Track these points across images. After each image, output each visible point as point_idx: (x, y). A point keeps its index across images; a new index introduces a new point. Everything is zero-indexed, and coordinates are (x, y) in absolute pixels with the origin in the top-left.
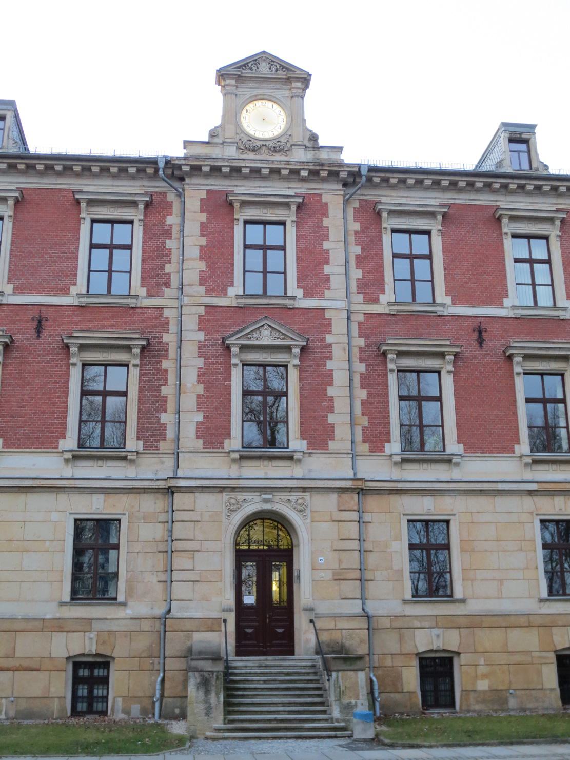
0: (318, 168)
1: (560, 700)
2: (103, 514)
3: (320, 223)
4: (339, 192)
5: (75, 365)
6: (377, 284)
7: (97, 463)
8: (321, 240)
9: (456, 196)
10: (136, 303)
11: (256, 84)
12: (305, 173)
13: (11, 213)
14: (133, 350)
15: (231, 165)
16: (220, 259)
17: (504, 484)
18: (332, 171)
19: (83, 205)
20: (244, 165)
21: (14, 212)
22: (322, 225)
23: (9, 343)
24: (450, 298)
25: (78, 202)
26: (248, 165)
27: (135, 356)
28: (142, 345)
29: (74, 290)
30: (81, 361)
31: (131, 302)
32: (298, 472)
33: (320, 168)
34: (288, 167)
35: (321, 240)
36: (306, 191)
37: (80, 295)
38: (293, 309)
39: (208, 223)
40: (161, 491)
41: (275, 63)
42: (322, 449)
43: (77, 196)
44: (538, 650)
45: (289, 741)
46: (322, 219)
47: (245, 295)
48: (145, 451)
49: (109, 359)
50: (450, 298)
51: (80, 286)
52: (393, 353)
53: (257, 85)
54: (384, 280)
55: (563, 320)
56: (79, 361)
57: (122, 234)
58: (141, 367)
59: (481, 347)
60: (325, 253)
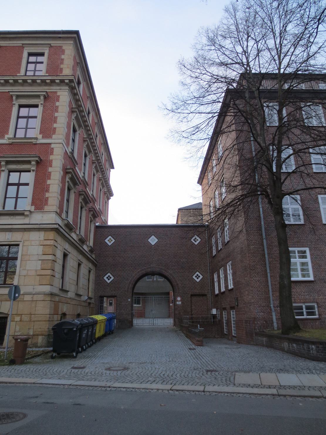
1: (5, 340)
5: (3, 171)
7: (11, 217)
9: (39, 88)
10: (36, 142)
13: (42, 102)
14: (32, 163)
17: (6, 226)
19: (14, 98)
21: (44, 102)
23: (39, 161)
24: (41, 136)
25: (12, 96)
26: (21, 78)
27: (33, 165)
28: (36, 160)
29: (6, 136)
30: (7, 169)
31: (34, 141)
32: (26, 221)
37: (9, 139)
38: (36, 144)
40: (55, 229)
42: (39, 210)
43: (11, 94)
44: (53, 313)
47: (25, 138)
48: (35, 211)
49: (21, 168)
50: (41, 136)
51: (11, 134)
52: (4, 162)
55: (35, 144)
56: (6, 169)
57: (33, 112)
58: (37, 171)
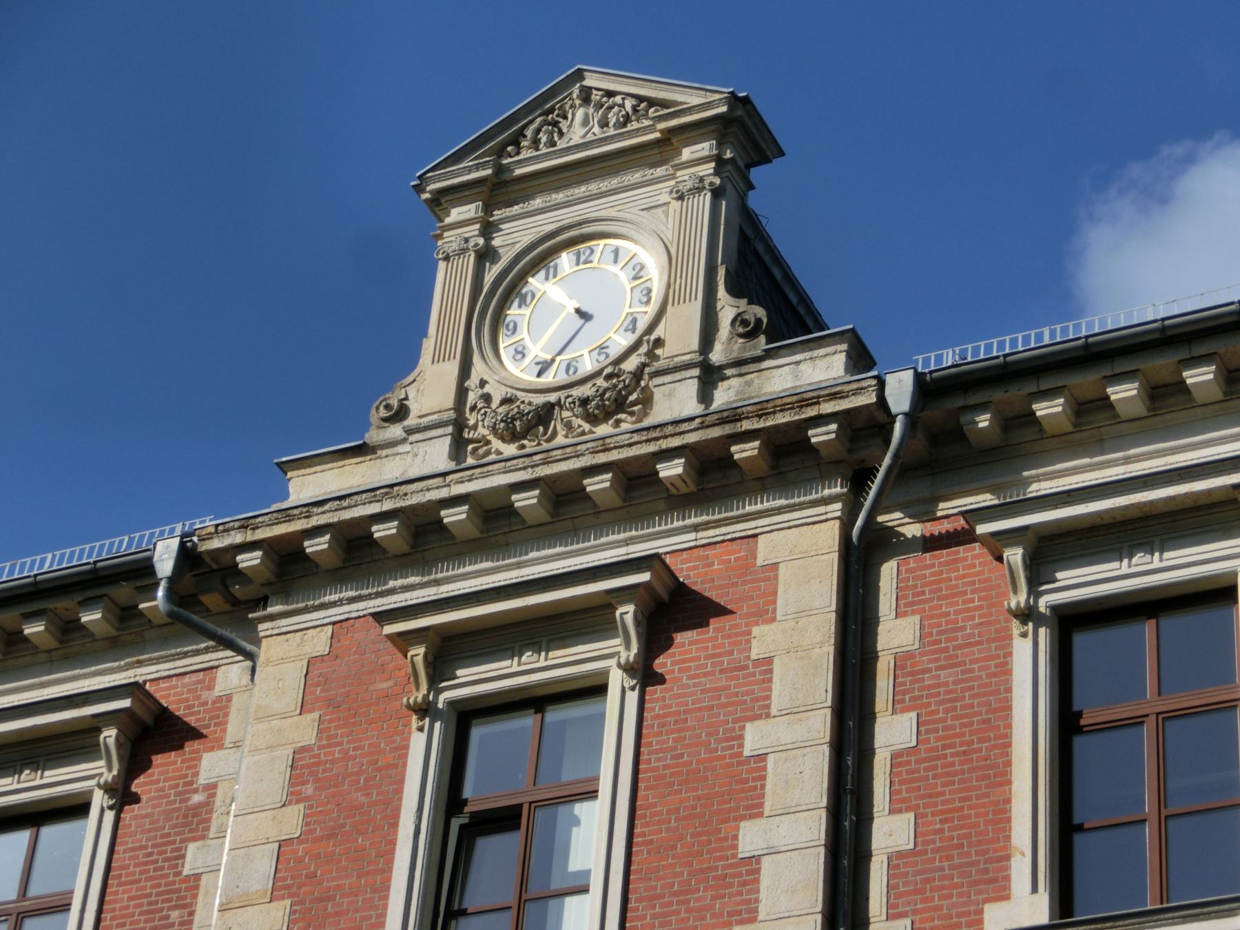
0: (716, 432)
2: (178, 668)
3: (740, 651)
4: (821, 509)
6: (977, 863)
8: (920, 853)
11: (557, 193)
12: (677, 466)
15: (400, 504)
16: (347, 877)
18: (777, 428)
20: (443, 493)
22: (748, 658)
33: (727, 429)
34: (602, 458)
35: (920, 853)
36: (692, 536)
39: (320, 748)
41: (618, 99)
45: (274, 527)
46: (749, 633)
53: (561, 195)
54: (1008, 838)
59: (731, 612)
60: (749, 771)
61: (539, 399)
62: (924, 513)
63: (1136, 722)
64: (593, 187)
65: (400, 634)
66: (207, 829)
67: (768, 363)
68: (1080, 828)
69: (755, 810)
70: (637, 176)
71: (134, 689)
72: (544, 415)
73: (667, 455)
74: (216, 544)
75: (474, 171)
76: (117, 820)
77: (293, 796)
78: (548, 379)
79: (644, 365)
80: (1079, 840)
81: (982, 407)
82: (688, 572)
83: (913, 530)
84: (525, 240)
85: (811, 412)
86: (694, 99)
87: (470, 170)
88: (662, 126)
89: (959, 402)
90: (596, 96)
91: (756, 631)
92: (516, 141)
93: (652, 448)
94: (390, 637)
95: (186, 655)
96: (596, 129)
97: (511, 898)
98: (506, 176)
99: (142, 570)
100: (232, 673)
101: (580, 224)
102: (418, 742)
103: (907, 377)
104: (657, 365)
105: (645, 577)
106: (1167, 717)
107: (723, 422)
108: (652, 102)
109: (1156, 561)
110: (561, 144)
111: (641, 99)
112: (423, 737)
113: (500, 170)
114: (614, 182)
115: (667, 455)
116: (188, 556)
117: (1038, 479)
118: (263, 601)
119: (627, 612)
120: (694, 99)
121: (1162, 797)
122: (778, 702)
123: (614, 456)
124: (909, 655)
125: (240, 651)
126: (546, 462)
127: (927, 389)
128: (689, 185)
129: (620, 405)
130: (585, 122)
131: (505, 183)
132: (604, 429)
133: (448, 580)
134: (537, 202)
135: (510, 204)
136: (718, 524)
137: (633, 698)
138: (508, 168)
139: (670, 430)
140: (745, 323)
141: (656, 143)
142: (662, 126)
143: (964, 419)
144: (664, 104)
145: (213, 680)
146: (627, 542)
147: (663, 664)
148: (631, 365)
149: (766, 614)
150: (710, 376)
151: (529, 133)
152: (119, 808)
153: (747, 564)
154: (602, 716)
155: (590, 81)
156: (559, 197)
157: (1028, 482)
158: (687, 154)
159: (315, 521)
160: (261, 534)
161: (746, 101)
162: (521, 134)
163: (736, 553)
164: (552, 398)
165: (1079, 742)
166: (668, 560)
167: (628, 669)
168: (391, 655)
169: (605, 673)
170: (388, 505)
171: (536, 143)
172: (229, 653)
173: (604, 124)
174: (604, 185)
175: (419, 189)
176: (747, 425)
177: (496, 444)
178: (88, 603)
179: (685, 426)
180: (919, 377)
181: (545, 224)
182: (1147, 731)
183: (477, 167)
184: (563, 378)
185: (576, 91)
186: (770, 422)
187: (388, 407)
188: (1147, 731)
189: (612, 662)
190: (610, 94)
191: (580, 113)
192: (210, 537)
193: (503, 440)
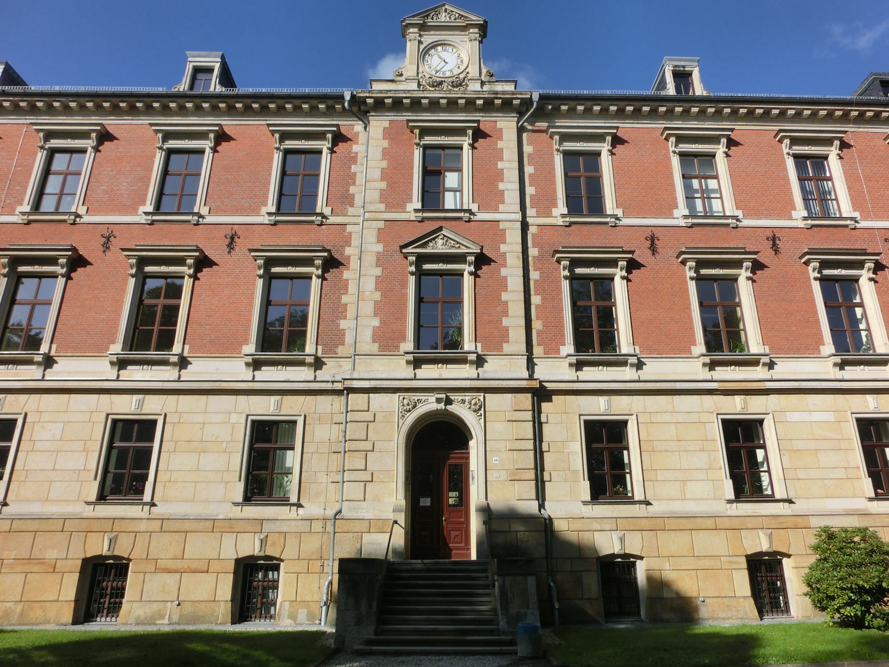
0: (492, 96)
20: (423, 95)
33: (495, 96)
34: (464, 96)
41: (454, 13)
61: (441, 79)
62: (532, 124)
63: (298, 175)
64: (447, 33)
65: (156, 130)
66: (357, 162)
67: (496, 83)
68: (164, 194)
69: (502, 180)
70: (458, 33)
71: (338, 126)
72: (441, 83)
73: (479, 98)
74: (361, 95)
75: (417, 20)
76: (213, 156)
77: (384, 159)
78: (438, 75)
79: (465, 77)
80: (283, 197)
81: (549, 104)
82: (110, 129)
83: (530, 127)
84: (430, 41)
85: (515, 96)
86: (474, 18)
87: (417, 20)
88: (467, 22)
89: (545, 102)
90: (448, 11)
91: (498, 142)
92: (428, 16)
93: (476, 96)
94: (153, 130)
95: (346, 121)
96: (448, 19)
97: (58, 191)
98: (425, 24)
99: (341, 98)
100: (358, 127)
101: (444, 40)
102: (39, 154)
103: (538, 94)
104: (469, 78)
105: (99, 128)
106: (305, 175)
107: (494, 94)
108: (462, 16)
109: (585, 144)
110: (438, 20)
111: (460, 15)
112: (41, 154)
113: (424, 22)
114: (452, 33)
115: (479, 98)
116: (353, 97)
117: (558, 122)
118: (369, 112)
119: (212, 136)
120: (474, 18)
121: (302, 191)
122: (505, 158)
123: (467, 96)
124: (531, 154)
125: (363, 122)
126: (450, 94)
127: (542, 97)
128: (473, 38)
129: (460, 85)
130: (445, 17)
131: (424, 26)
132: (455, 89)
133: (420, 116)
134: (432, 33)
135: (425, 31)
136: (488, 117)
137: (93, 154)
138: (426, 22)
139: (481, 93)
140: (490, 73)
141: (464, 26)
142: (467, 22)
143: (546, 106)
144: (466, 17)
145: (353, 128)
146: (466, 116)
147: (219, 148)
148: (462, 76)
149: (500, 138)
150: (483, 83)
151: (431, 15)
152: (331, 153)
153: (495, 127)
154: (85, 158)
155: (447, 7)
156: (438, 33)
157: (556, 122)
158: (471, 30)
159: (388, 95)
160: (373, 95)
161: (487, 22)
162: (429, 15)
163: (492, 124)
164: (443, 79)
165: (285, 177)
166: (224, 127)
167: (211, 148)
168: (35, 133)
169: (87, 148)
170: (408, 95)
171: (432, 18)
172: (361, 122)
173: (450, 18)
174: (449, 33)
175: (402, 22)
176: (499, 96)
177: (428, 87)
178: (321, 103)
179: (484, 93)
180: (540, 94)
181: (436, 38)
182: (300, 177)
183: (419, 20)
184: (441, 75)
185: (444, 9)
186: (505, 96)
187: (399, 72)
188: (300, 177)
189: (207, 146)
190: (452, 11)
191: (444, 14)
192: (360, 93)
193: (430, 86)
